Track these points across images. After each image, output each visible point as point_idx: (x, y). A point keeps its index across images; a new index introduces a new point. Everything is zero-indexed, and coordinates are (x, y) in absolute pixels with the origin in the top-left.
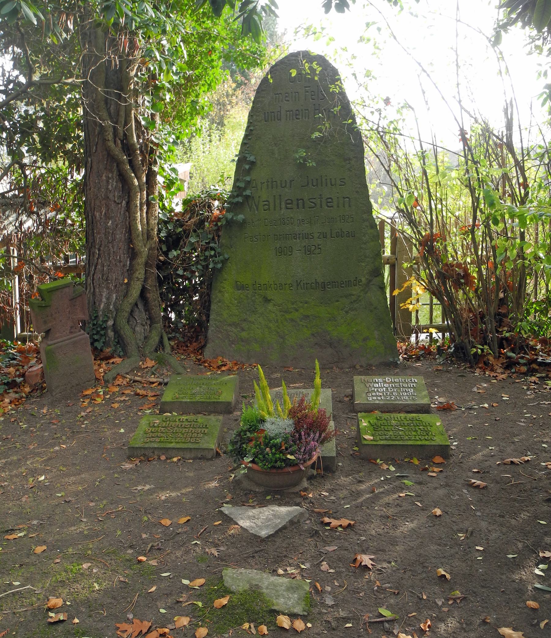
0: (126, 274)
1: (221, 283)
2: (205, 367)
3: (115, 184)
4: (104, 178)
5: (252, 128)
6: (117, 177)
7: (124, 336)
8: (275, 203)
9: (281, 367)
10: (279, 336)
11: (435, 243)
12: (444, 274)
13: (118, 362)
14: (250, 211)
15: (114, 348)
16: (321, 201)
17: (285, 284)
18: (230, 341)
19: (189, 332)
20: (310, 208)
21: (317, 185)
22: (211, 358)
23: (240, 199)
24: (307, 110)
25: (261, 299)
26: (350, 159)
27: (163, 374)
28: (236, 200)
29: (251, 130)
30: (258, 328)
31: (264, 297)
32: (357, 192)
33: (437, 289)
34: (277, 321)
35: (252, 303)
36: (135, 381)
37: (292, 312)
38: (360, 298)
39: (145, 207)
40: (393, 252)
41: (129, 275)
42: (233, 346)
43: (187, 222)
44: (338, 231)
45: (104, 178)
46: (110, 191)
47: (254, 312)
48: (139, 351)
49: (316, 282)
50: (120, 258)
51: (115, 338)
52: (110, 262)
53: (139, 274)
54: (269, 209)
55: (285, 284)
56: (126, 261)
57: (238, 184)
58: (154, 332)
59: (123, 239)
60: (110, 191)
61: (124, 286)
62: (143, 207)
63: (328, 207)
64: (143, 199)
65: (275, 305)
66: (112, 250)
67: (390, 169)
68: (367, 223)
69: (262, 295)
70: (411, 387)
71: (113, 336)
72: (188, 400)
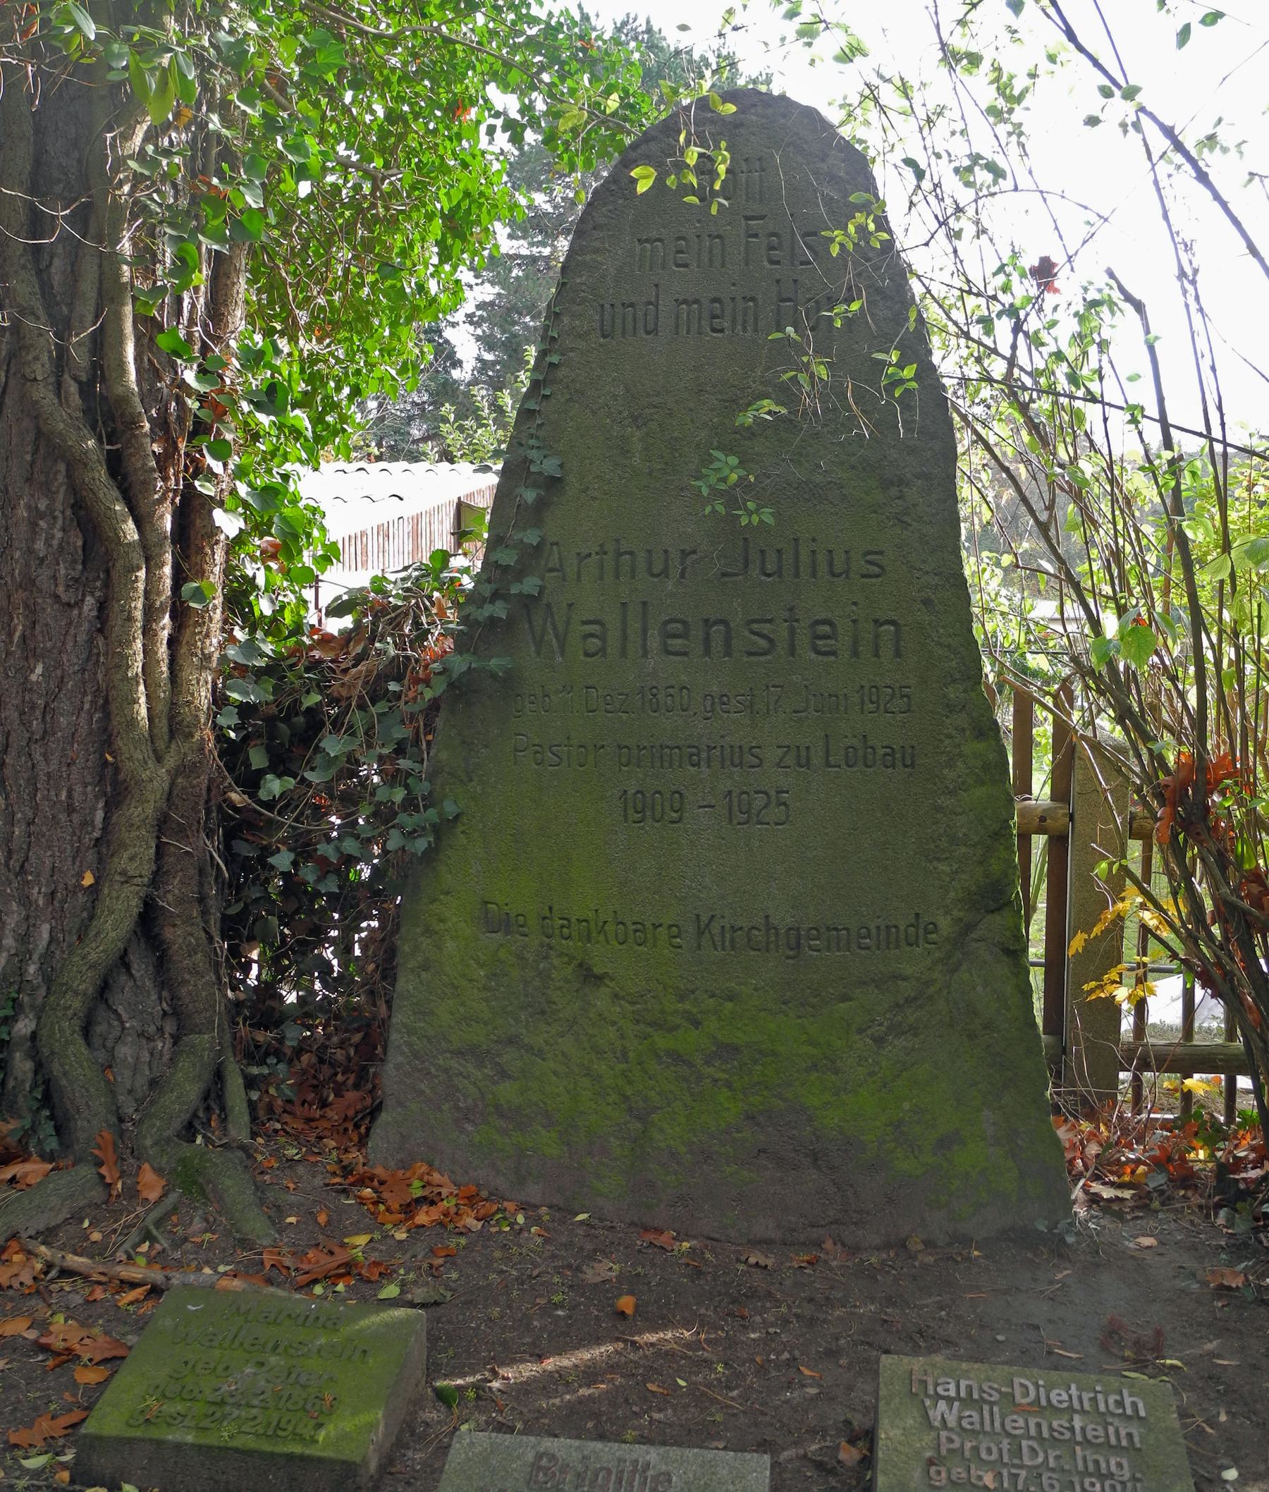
0: (91, 856)
1: (433, 901)
2: (362, 1201)
3: (59, 535)
4: (22, 512)
5: (555, 359)
6: (69, 512)
7: (64, 1082)
8: (624, 631)
9: (632, 1224)
10: (630, 1109)
11: (1216, 798)
12: (1245, 913)
13: (32, 1180)
14: (538, 652)
15: (27, 1123)
16: (792, 632)
17: (656, 927)
18: (458, 1109)
19: (341, 1045)
20: (750, 654)
21: (779, 572)
22: (392, 1164)
23: (499, 610)
24: (753, 299)
25: (569, 970)
26: (901, 482)
27: (186, 1240)
28: (488, 610)
29: (551, 364)
30: (555, 1073)
31: (581, 965)
32: (927, 602)
33: (1219, 964)
34: (625, 1053)
35: (537, 983)
36: (66, 1273)
37: (677, 1027)
38: (932, 990)
39: (166, 620)
40: (1060, 792)
41: (100, 860)
42: (470, 1128)
43: (345, 671)
44: (855, 742)
45: (22, 512)
46: (42, 560)
47: (543, 1012)
48: (121, 1134)
49: (769, 926)
50: (70, 796)
51: (35, 1086)
52: (36, 808)
53: (131, 859)
54: (602, 651)
55: (656, 927)
56: (93, 809)
57: (493, 558)
58: (184, 1063)
59: (83, 731)
60: (42, 560)
61: (81, 898)
62: (157, 621)
63: (818, 652)
64: (159, 593)
65: (616, 996)
66: (42, 765)
67: (1052, 517)
68: (961, 719)
69: (572, 958)
70: (1118, 1449)
71: (30, 1075)
72: (190, 1438)
